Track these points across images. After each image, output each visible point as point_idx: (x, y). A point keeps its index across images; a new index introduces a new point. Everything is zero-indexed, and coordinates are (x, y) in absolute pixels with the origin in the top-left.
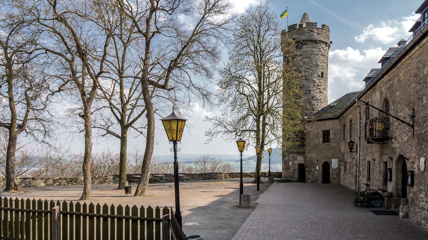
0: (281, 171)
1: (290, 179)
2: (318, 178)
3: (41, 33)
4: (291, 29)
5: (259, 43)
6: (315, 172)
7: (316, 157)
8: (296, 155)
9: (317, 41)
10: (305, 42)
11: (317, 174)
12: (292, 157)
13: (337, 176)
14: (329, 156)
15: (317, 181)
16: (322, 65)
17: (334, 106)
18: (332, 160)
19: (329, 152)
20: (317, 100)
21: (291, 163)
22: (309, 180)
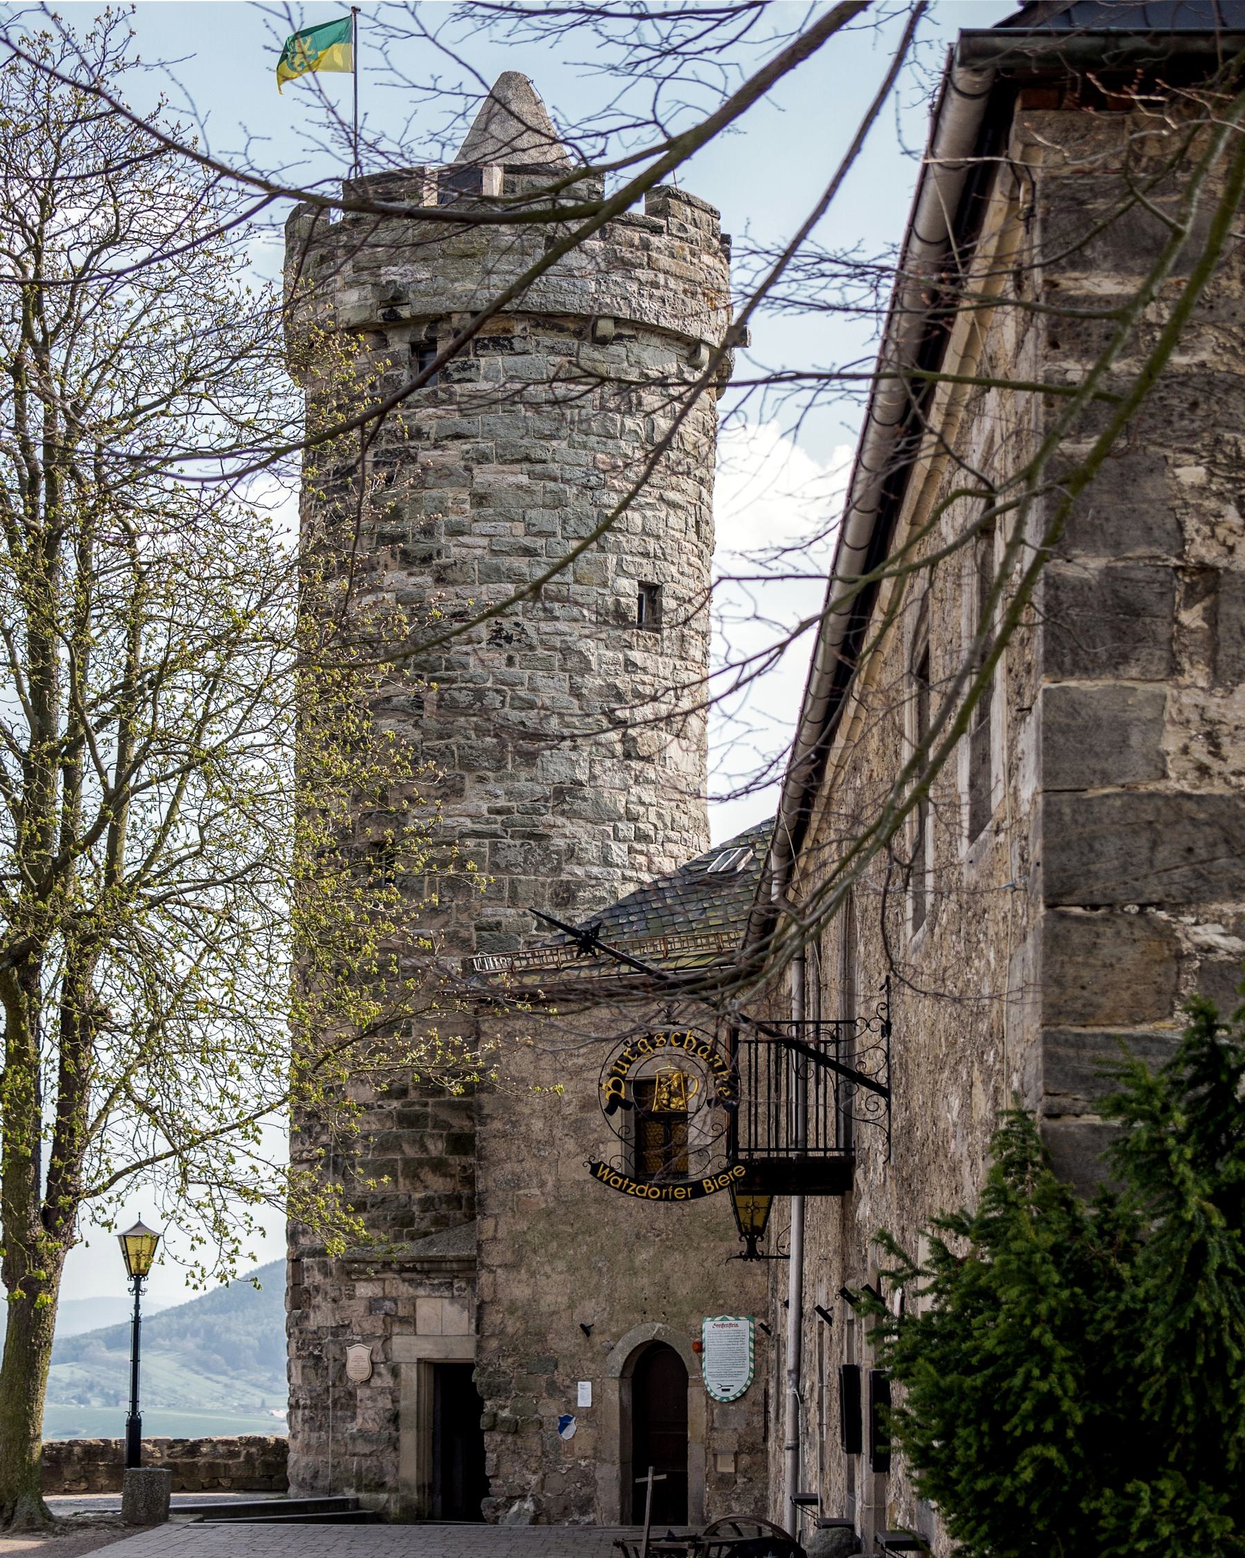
0: (284, 1433)
1: (350, 1494)
2: (587, 1478)
5: (34, 343)
6: (568, 1434)
7: (571, 1306)
8: (405, 1290)
9: (606, 327)
11: (585, 1445)
12: (373, 1305)
13: (745, 1460)
14: (683, 1290)
15: (586, 1505)
16: (652, 525)
17: (730, 875)
18: (708, 1325)
19: (678, 1257)
20: (602, 815)
21: (358, 1358)
22: (511, 1500)
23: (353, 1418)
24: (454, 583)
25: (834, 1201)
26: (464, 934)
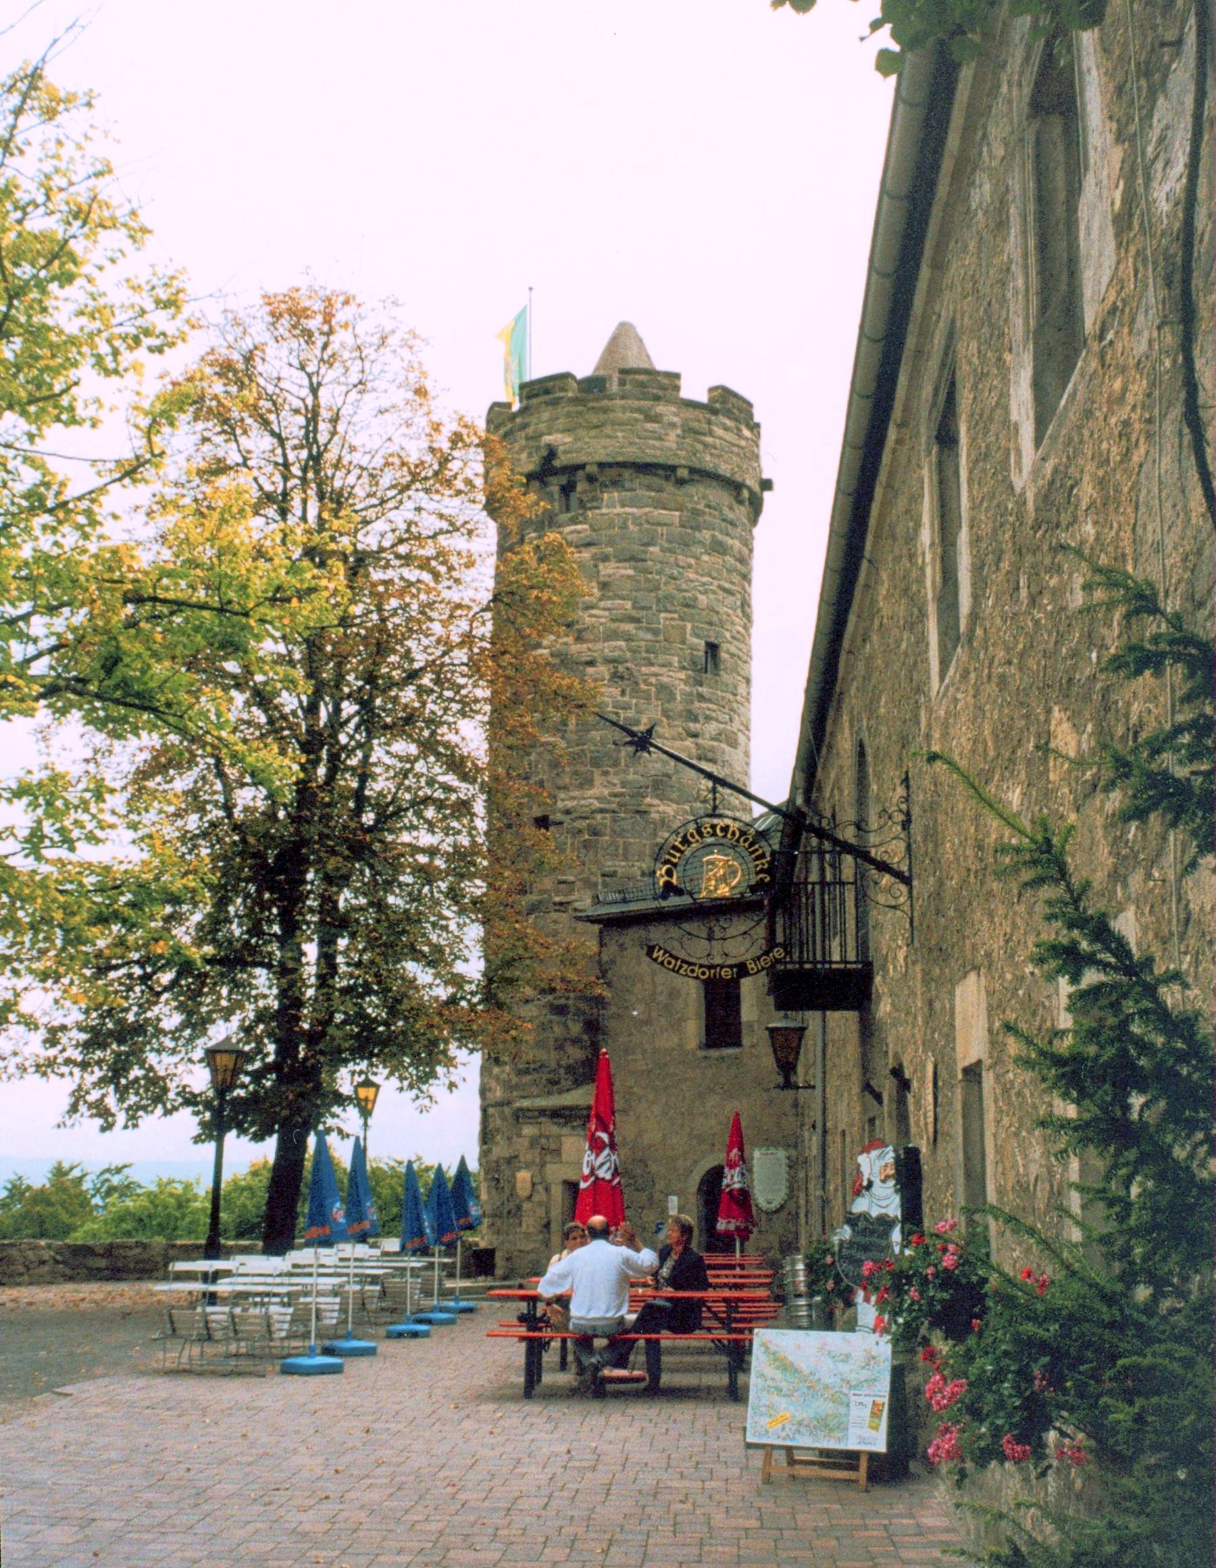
3: (742, 1158)
4: (534, 401)
9: (683, 473)
10: (613, 472)
12: (534, 1142)
23: (520, 1225)
24: (587, 641)
25: (851, 1016)
26: (593, 879)
